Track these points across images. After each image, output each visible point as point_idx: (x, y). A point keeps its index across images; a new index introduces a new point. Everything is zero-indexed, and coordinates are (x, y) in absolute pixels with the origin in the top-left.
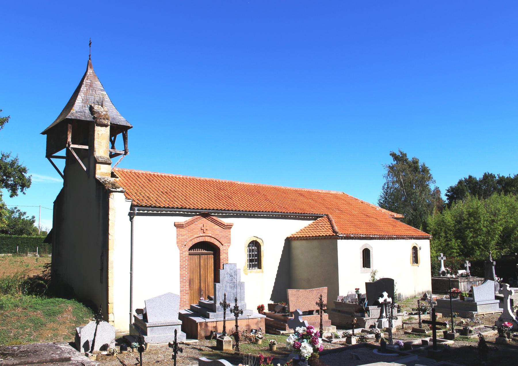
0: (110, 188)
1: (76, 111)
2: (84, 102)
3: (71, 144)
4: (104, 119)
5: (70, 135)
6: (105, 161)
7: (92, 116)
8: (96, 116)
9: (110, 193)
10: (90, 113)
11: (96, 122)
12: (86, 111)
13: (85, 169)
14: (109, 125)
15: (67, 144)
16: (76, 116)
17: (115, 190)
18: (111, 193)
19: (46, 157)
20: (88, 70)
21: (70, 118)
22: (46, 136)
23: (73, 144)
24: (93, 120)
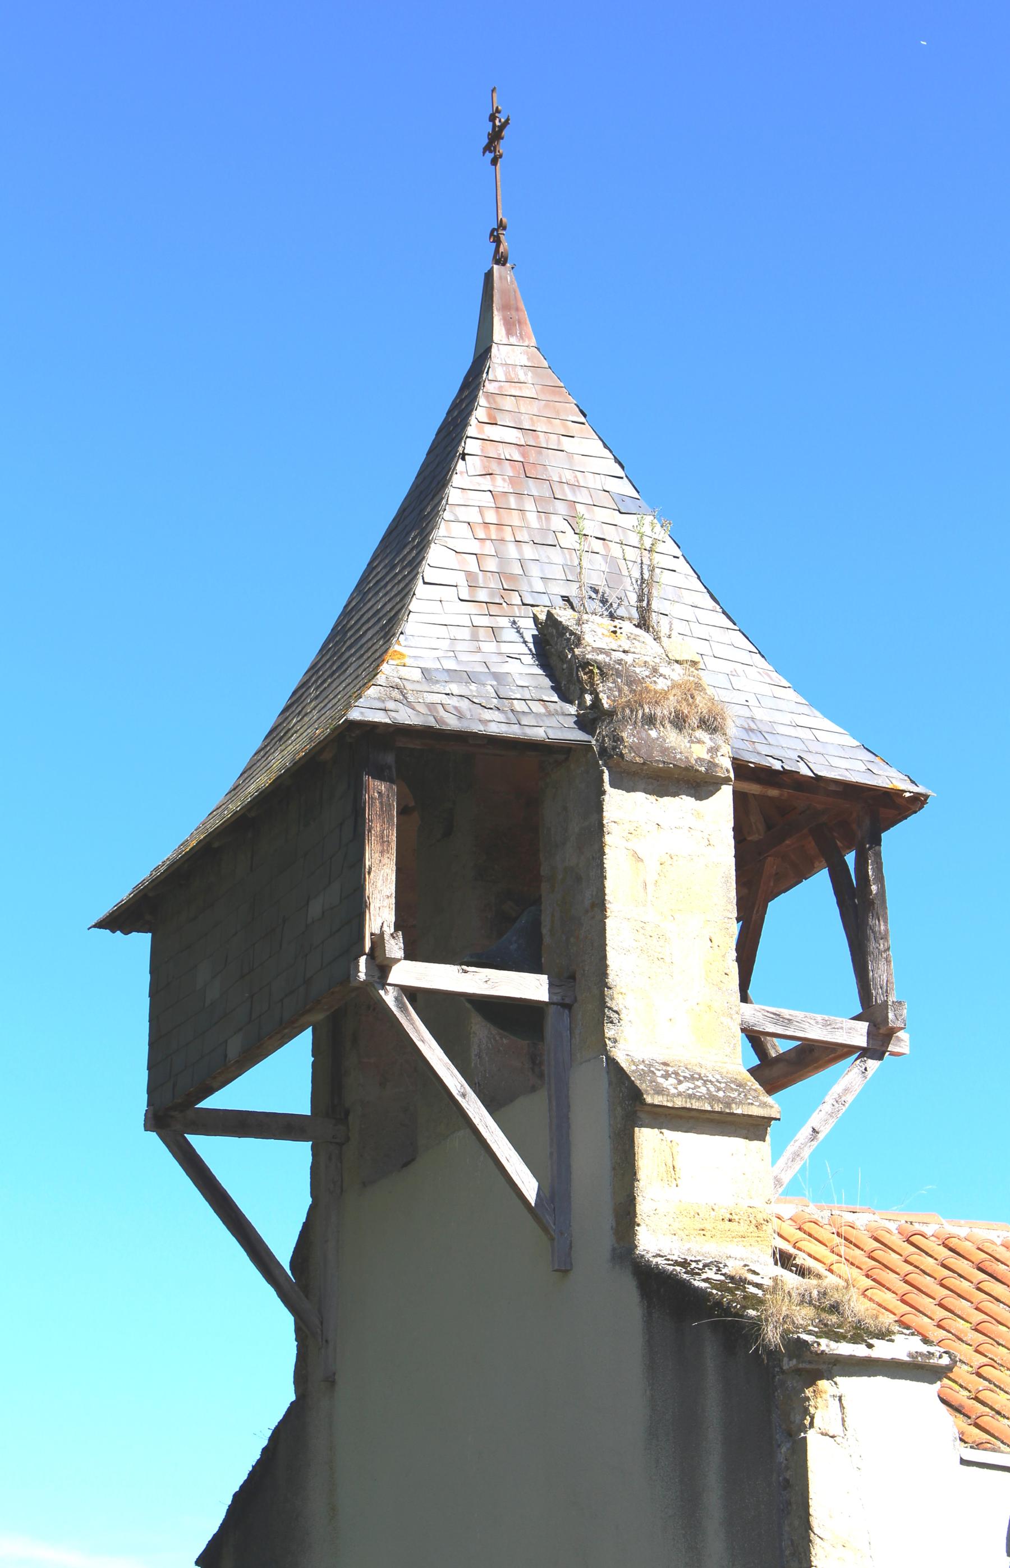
0: (810, 1333)
1: (424, 671)
2: (482, 595)
3: (399, 954)
4: (679, 722)
5: (385, 880)
6: (719, 1100)
7: (572, 709)
8: (606, 703)
9: (812, 1383)
10: (547, 682)
11: (610, 754)
12: (512, 667)
13: (529, 1186)
14: (726, 781)
15: (363, 960)
16: (431, 706)
17: (860, 1351)
18: (823, 1384)
19: (146, 1130)
20: (494, 349)
21: (380, 717)
22: (141, 943)
23: (411, 954)
24: (580, 736)
